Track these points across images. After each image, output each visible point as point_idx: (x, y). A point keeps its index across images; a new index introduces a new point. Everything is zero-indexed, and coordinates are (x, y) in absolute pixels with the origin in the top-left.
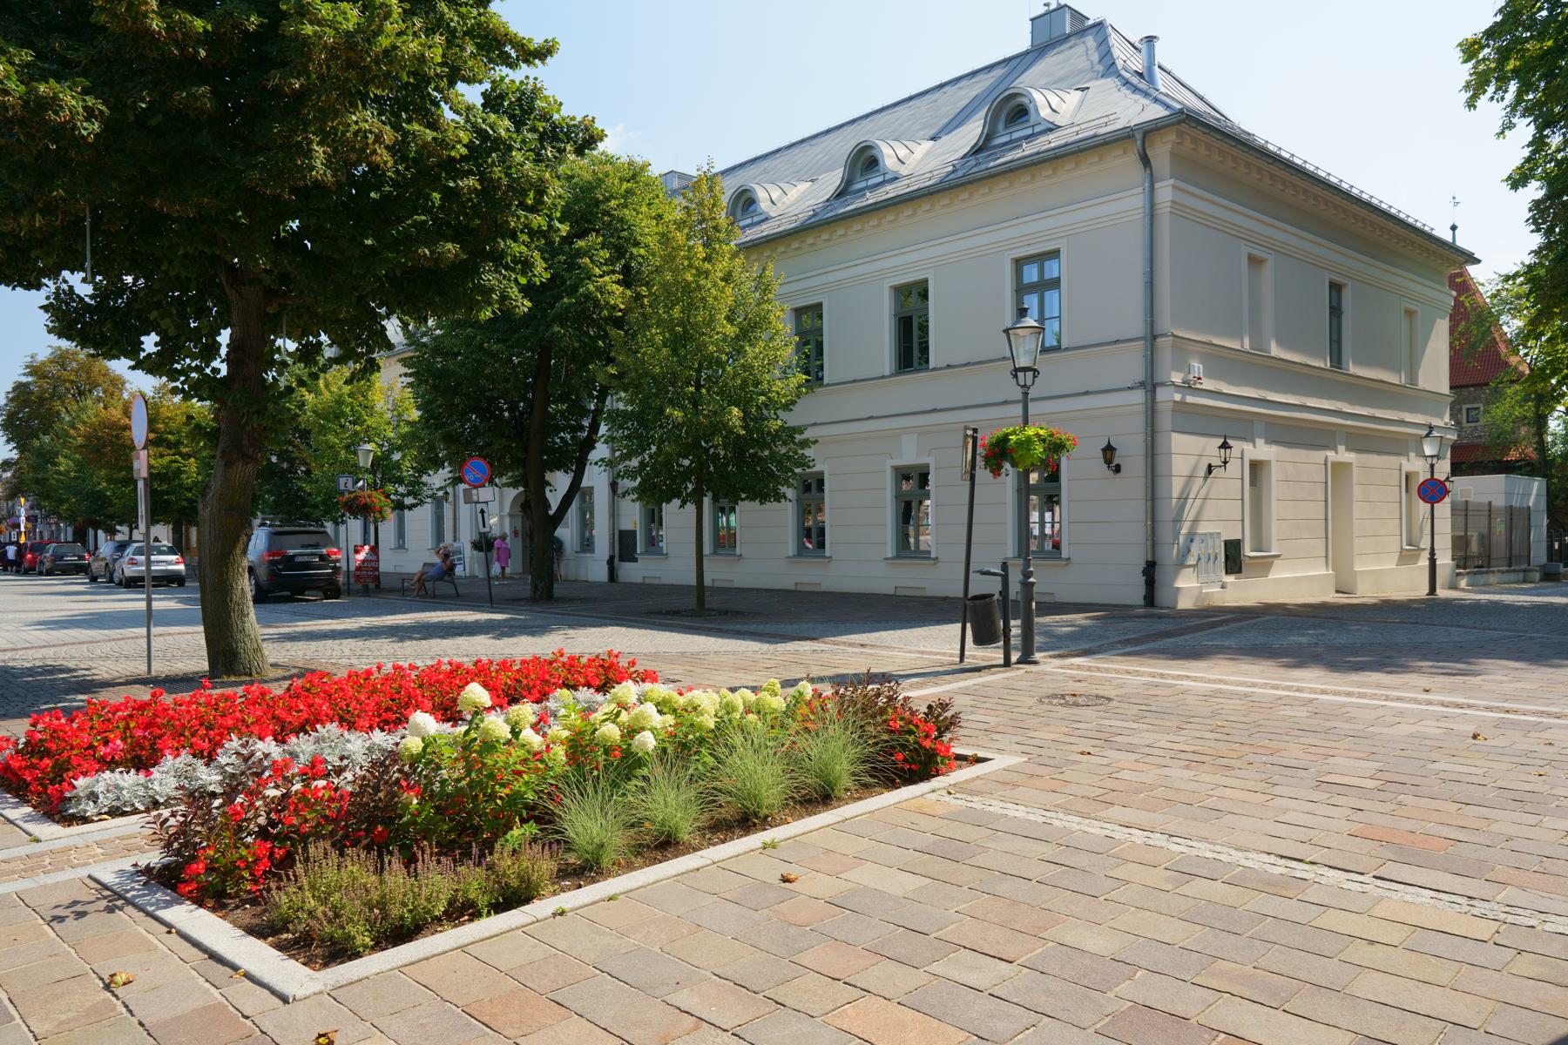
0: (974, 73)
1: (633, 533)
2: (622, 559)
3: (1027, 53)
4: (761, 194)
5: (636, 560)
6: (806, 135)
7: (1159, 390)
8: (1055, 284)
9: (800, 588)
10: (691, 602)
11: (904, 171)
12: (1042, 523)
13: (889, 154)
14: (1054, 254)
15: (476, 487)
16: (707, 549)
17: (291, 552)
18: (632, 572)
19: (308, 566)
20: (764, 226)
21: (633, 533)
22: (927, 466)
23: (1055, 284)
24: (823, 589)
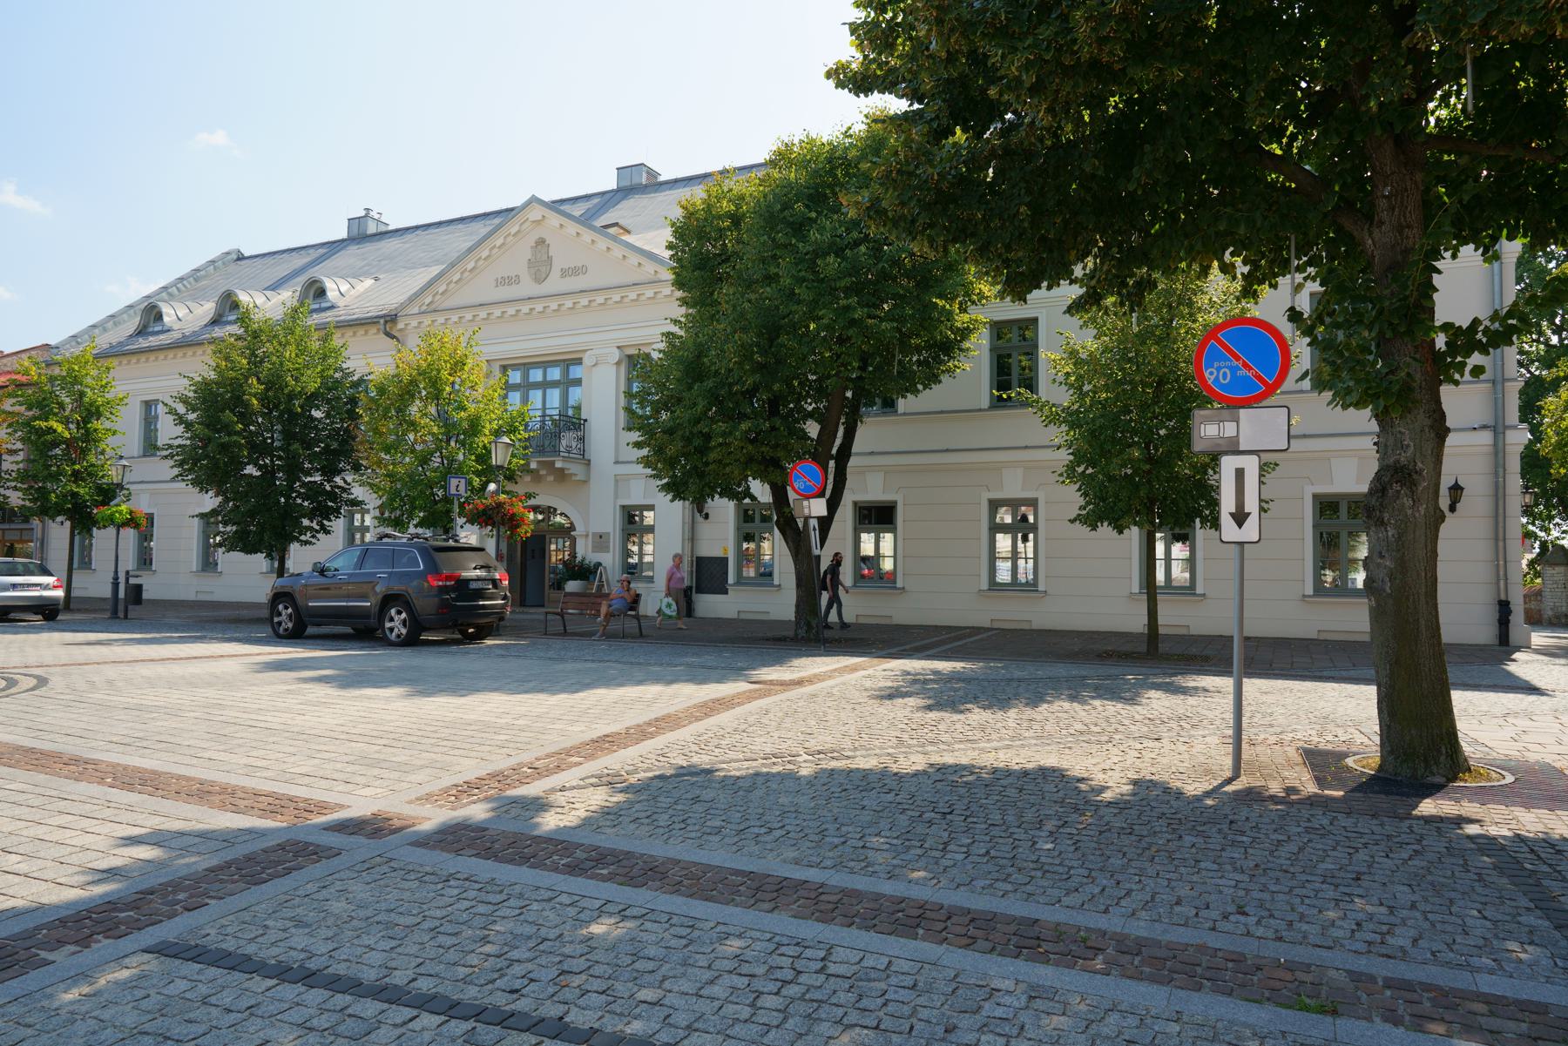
0: (486, 215)
1: (723, 561)
2: (699, 591)
3: (343, 241)
4: (329, 285)
5: (726, 592)
6: (680, 175)
7: (1508, 433)
8: (578, 382)
9: (743, 616)
10: (1143, 648)
11: (341, 303)
12: (1015, 556)
13: (169, 315)
14: (579, 361)
15: (808, 498)
16: (75, 565)
17: (466, 574)
18: (710, 605)
19: (480, 594)
20: (329, 313)
21: (723, 561)
22: (1315, 496)
23: (578, 382)
24: (1035, 626)
